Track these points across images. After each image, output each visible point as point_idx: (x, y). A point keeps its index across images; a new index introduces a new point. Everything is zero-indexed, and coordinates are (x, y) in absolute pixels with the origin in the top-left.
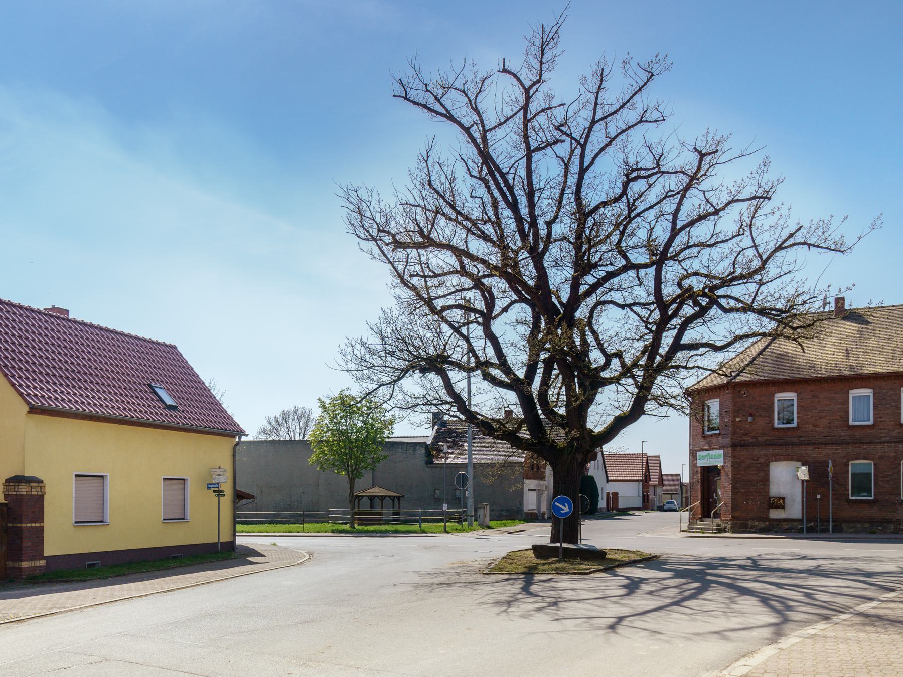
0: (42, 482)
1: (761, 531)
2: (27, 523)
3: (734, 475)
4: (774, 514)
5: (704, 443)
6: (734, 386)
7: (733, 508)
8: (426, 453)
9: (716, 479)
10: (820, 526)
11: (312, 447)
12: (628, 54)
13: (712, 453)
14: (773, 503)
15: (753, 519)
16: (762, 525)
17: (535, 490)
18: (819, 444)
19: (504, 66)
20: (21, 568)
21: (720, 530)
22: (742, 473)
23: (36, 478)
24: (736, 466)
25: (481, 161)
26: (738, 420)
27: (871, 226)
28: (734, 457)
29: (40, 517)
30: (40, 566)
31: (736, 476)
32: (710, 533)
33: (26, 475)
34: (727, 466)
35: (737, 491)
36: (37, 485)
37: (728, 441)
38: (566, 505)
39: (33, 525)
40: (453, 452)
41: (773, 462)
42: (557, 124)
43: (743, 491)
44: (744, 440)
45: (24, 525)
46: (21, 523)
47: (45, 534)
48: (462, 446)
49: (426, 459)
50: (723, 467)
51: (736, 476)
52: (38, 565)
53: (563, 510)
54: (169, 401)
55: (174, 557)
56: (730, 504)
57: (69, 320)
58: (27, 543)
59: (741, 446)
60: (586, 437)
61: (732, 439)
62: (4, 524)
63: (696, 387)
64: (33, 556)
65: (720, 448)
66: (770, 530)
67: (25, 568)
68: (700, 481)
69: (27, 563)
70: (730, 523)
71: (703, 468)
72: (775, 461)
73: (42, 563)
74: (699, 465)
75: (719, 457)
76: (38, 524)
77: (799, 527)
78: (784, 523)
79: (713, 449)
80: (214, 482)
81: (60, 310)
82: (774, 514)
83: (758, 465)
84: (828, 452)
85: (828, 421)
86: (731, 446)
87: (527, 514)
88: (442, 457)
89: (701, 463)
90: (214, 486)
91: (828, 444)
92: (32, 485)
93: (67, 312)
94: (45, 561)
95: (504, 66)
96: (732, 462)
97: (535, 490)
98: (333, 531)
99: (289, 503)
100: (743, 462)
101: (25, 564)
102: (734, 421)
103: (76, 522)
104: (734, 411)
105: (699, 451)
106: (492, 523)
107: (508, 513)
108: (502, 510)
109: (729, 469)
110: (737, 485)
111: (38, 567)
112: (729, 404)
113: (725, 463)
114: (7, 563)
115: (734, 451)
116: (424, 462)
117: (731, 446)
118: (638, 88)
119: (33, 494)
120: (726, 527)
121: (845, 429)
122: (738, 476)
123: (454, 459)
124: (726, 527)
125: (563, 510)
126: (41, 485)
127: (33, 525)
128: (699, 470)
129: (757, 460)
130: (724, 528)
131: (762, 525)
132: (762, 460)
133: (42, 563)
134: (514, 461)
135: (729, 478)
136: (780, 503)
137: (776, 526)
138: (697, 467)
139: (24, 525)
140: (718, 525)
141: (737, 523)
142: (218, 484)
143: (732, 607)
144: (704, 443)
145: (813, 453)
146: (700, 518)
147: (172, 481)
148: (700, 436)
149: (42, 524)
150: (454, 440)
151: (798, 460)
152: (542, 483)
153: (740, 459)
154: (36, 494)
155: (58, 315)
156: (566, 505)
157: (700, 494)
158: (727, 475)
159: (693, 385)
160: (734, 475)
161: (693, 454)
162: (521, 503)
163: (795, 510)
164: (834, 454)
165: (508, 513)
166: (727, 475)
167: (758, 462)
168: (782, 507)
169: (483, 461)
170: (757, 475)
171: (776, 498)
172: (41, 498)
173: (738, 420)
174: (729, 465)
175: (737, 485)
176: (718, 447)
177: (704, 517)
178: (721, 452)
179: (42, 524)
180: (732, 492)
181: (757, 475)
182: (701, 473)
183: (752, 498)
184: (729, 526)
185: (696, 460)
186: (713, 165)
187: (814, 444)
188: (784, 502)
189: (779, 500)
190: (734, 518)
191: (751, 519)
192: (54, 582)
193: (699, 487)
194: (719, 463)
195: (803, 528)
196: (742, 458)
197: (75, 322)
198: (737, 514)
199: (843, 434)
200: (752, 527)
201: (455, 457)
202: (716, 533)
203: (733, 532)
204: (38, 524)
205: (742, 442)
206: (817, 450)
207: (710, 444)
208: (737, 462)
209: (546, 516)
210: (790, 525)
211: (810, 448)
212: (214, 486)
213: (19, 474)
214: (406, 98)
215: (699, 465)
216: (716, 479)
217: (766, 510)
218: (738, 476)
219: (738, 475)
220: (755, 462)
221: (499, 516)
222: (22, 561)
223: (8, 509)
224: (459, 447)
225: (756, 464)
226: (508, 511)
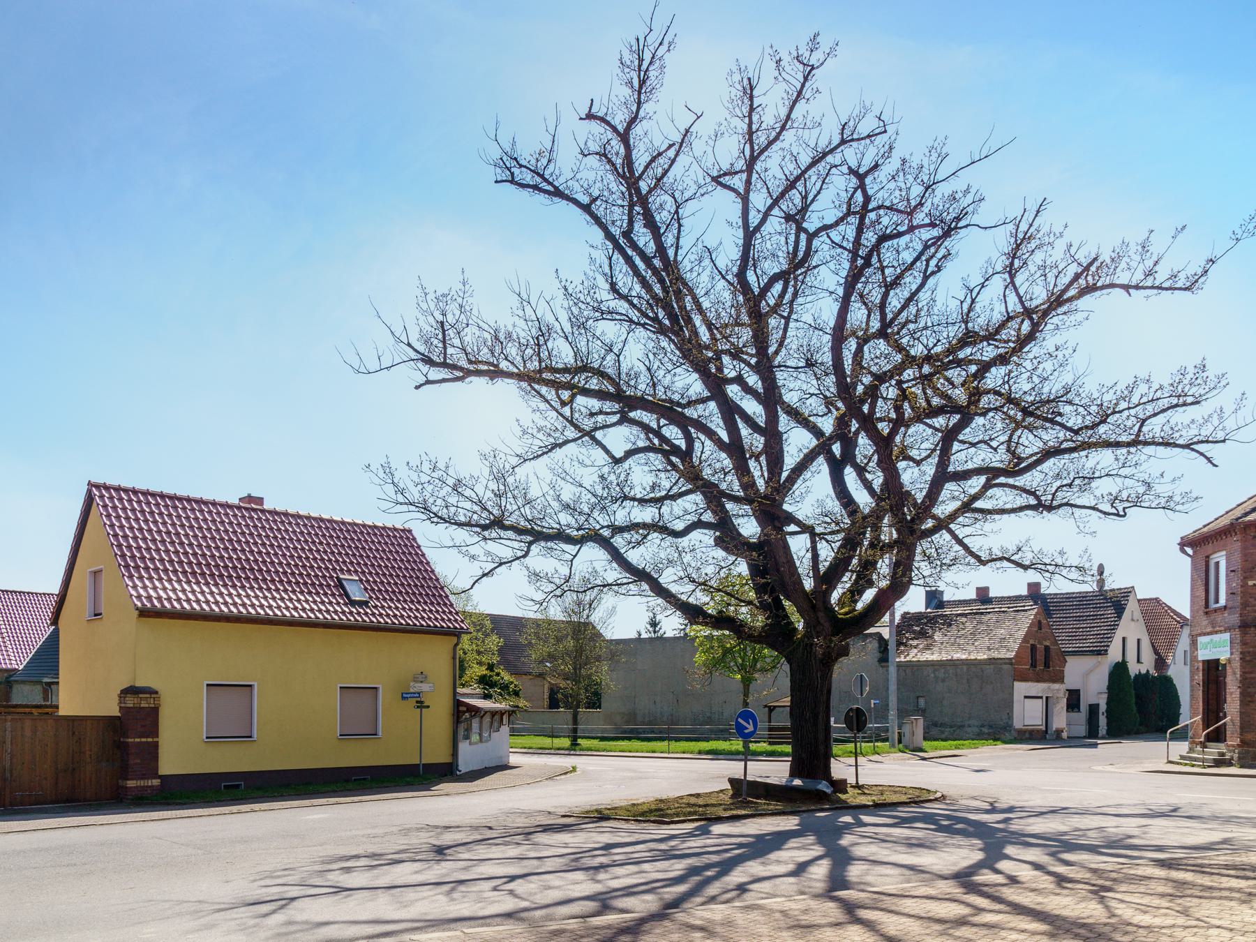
0: (156, 693)
2: (134, 738)
3: (1244, 673)
5: (1206, 622)
6: (1245, 528)
7: (1242, 728)
8: (880, 647)
11: (696, 644)
12: (772, 47)
13: (1216, 637)
17: (1041, 697)
19: (590, 108)
20: (127, 787)
21: (1219, 763)
23: (150, 688)
24: (1248, 658)
25: (612, 247)
26: (1251, 583)
27: (1233, 237)
28: (1244, 643)
29: (154, 730)
30: (152, 786)
31: (1248, 676)
32: (1199, 766)
33: (137, 685)
35: (1249, 699)
36: (148, 696)
37: (1234, 619)
38: (751, 721)
39: (144, 740)
40: (918, 645)
42: (715, 174)
45: (130, 740)
46: (128, 737)
47: (160, 751)
48: (931, 637)
49: (879, 655)
50: (1229, 661)
51: (1248, 676)
52: (150, 784)
53: (747, 728)
54: (357, 596)
55: (355, 780)
57: (263, 511)
58: (134, 761)
60: (822, 621)
61: (1241, 615)
62: (116, 739)
64: (143, 775)
65: (1225, 631)
67: (131, 787)
68: (1201, 683)
69: (135, 782)
70: (1237, 751)
73: (156, 782)
76: (150, 740)
79: (1216, 632)
80: (412, 690)
81: (250, 499)
86: (1240, 627)
87: (1020, 732)
88: (902, 652)
90: (412, 695)
92: (141, 696)
93: (260, 501)
94: (159, 781)
95: (590, 108)
96: (1241, 653)
97: (1041, 697)
98: (700, 752)
99: (708, 714)
101: (131, 783)
102: (1244, 585)
103: (207, 738)
104: (1245, 570)
105: (1200, 635)
106: (926, 744)
107: (990, 731)
108: (983, 726)
109: (1237, 664)
110: (1249, 690)
111: (150, 787)
112: (1237, 557)
113: (1232, 654)
114: (120, 781)
115: (1244, 634)
116: (876, 660)
118: (795, 94)
119: (142, 706)
120: (1232, 758)
123: (916, 655)
124: (1232, 758)
125: (747, 728)
126: (155, 696)
127: (144, 740)
128: (1201, 664)
130: (1230, 760)
133: (156, 782)
134: (999, 656)
138: (1198, 662)
139: (130, 740)
140: (1223, 754)
141: (1248, 752)
142: (419, 693)
144: (1206, 622)
147: (361, 690)
148: (1201, 613)
149: (155, 740)
150: (922, 628)
152: (1056, 686)
154: (147, 705)
155: (252, 503)
156: (751, 721)
157: (1201, 704)
158: (1235, 673)
160: (1243, 674)
162: (1010, 716)
165: (990, 731)
166: (1235, 673)
169: (956, 656)
172: (155, 711)
173: (1251, 583)
174: (1237, 657)
175: (1249, 690)
177: (1209, 741)
178: (1227, 636)
179: (155, 740)
180: (1241, 701)
182: (1203, 670)
186: (929, 187)
192: (156, 804)
193: (1200, 693)
194: (1223, 654)
197: (274, 513)
198: (1249, 737)
201: (919, 652)
202: (1209, 767)
203: (1242, 767)
204: (150, 740)
207: (1213, 624)
208: (1249, 652)
209: (1065, 735)
212: (412, 695)
213: (132, 684)
214: (512, 181)
215: (1200, 659)
221: (978, 735)
222: (128, 779)
223: (121, 722)
224: (929, 637)
226: (991, 727)
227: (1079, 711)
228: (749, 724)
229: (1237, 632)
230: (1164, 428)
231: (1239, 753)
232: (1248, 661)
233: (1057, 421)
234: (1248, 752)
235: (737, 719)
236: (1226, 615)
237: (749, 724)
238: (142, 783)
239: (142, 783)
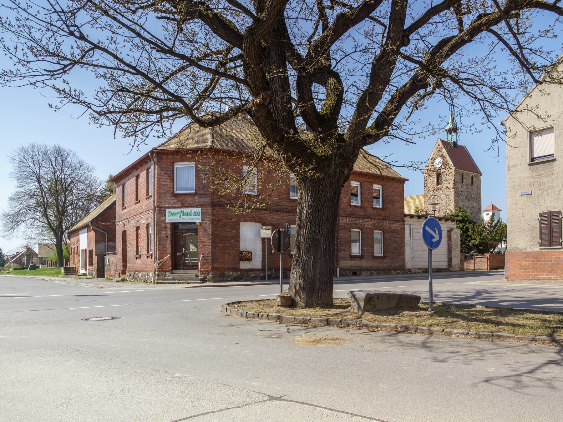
1: (235, 280)
3: (213, 231)
4: (244, 265)
9: (184, 235)
10: (275, 274)
14: (244, 256)
15: (229, 270)
16: (236, 274)
18: (272, 211)
21: (204, 280)
22: (220, 229)
28: (213, 215)
31: (215, 232)
34: (206, 223)
41: (242, 222)
43: (220, 245)
44: (221, 201)
50: (201, 224)
51: (215, 232)
56: (210, 257)
59: (219, 206)
63: (161, 148)
65: (197, 206)
66: (242, 279)
68: (169, 236)
71: (175, 226)
72: (244, 221)
74: (167, 221)
75: (196, 214)
77: (261, 275)
78: (251, 273)
82: (244, 265)
83: (232, 224)
84: (278, 217)
85: (278, 194)
89: (170, 219)
91: (278, 211)
100: (220, 220)
105: (169, 208)
109: (208, 225)
110: (216, 240)
113: (203, 220)
115: (213, 209)
117: (211, 205)
121: (288, 200)
122: (217, 232)
128: (169, 226)
129: (231, 219)
131: (236, 274)
132: (234, 220)
135: (208, 234)
136: (247, 257)
137: (245, 275)
138: (165, 223)
141: (216, 274)
143: (497, 342)
145: (276, 217)
146: (171, 270)
151: (259, 222)
153: (218, 217)
159: (159, 146)
160: (213, 231)
161: (160, 211)
163: (257, 263)
164: (281, 219)
167: (232, 221)
168: (250, 259)
170: (231, 232)
171: (246, 252)
174: (208, 222)
175: (216, 240)
176: (194, 205)
178: (199, 210)
180: (212, 246)
181: (231, 232)
183: (227, 251)
184: (210, 276)
185: (165, 216)
187: (270, 210)
188: (251, 255)
189: (248, 254)
190: (214, 269)
191: (227, 270)
193: (169, 242)
194: (198, 219)
195: (265, 276)
196: (220, 217)
198: (216, 265)
199: (286, 204)
200: (228, 276)
203: (214, 282)
205: (219, 203)
206: (271, 215)
207: (182, 202)
208: (215, 220)
210: (255, 274)
211: (268, 213)
216: (184, 235)
217: (238, 262)
218: (217, 232)
219: (216, 231)
220: (229, 221)
225: (231, 222)
227: (115, 253)
228: (436, 233)
229: (209, 209)
230: (541, 80)
231: (212, 274)
232: (215, 225)
233: (530, 71)
234: (216, 274)
235: (424, 229)
236: (196, 198)
237: (435, 232)
238: (266, 252)
239: (266, 252)
